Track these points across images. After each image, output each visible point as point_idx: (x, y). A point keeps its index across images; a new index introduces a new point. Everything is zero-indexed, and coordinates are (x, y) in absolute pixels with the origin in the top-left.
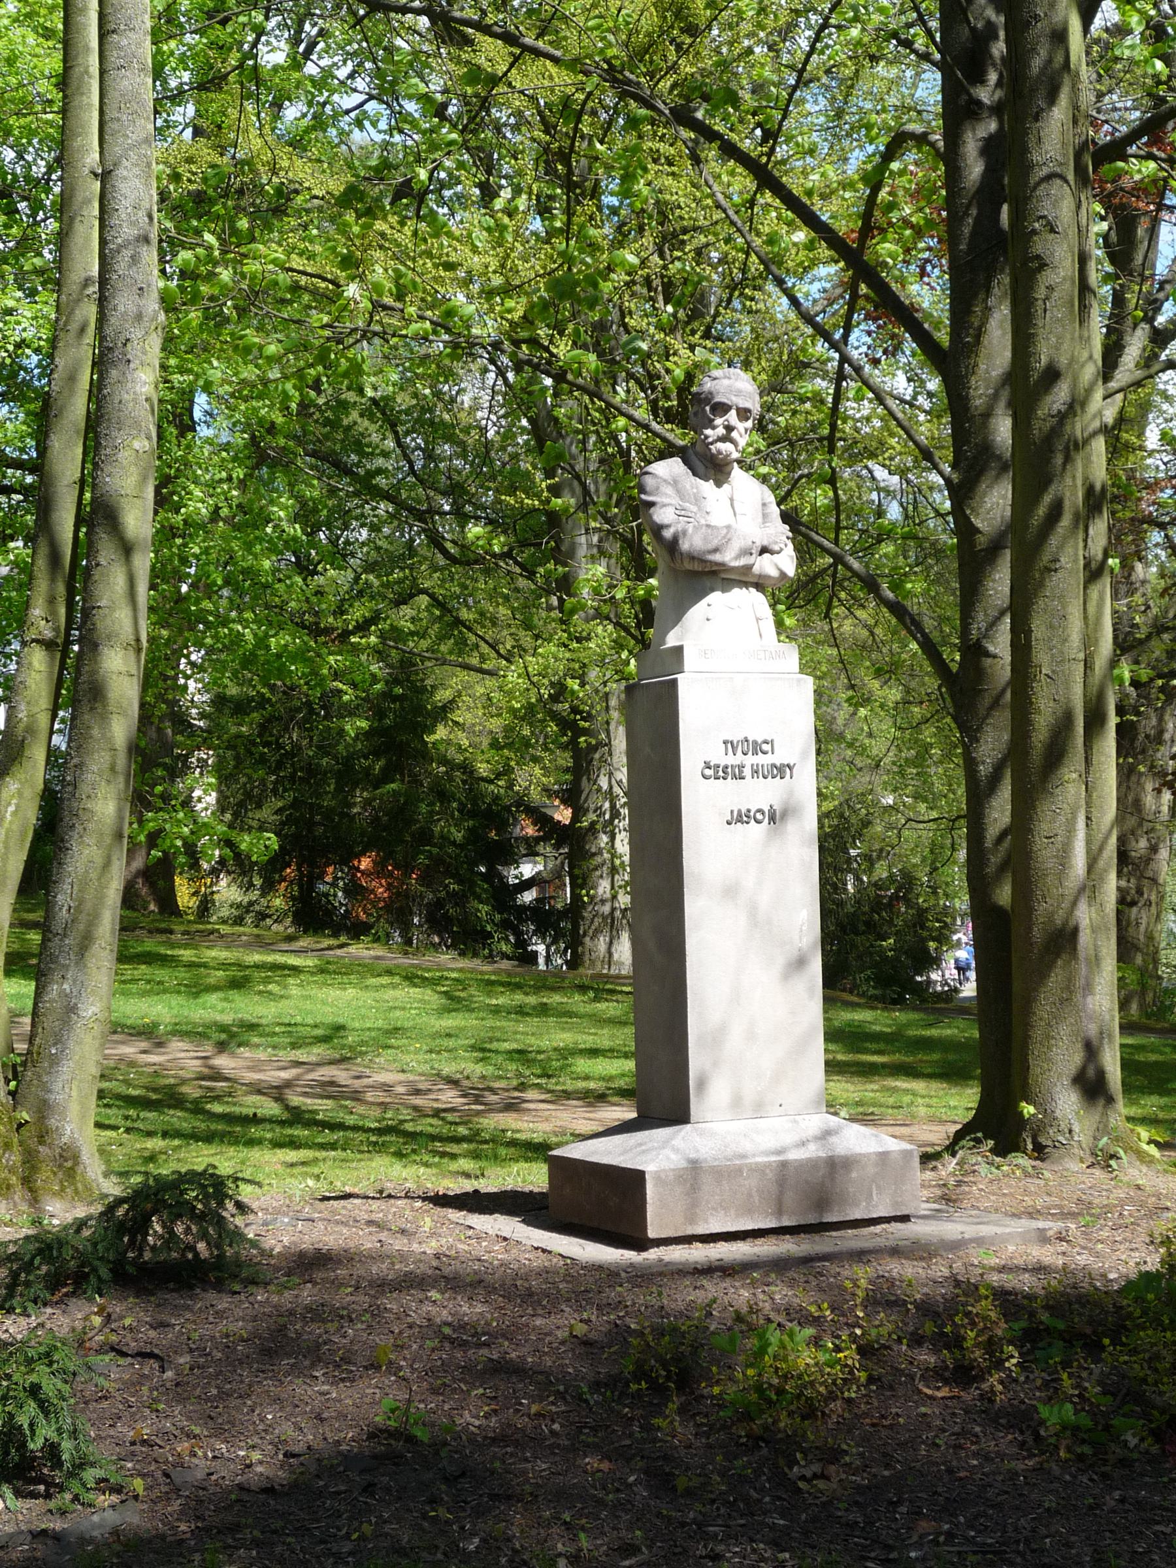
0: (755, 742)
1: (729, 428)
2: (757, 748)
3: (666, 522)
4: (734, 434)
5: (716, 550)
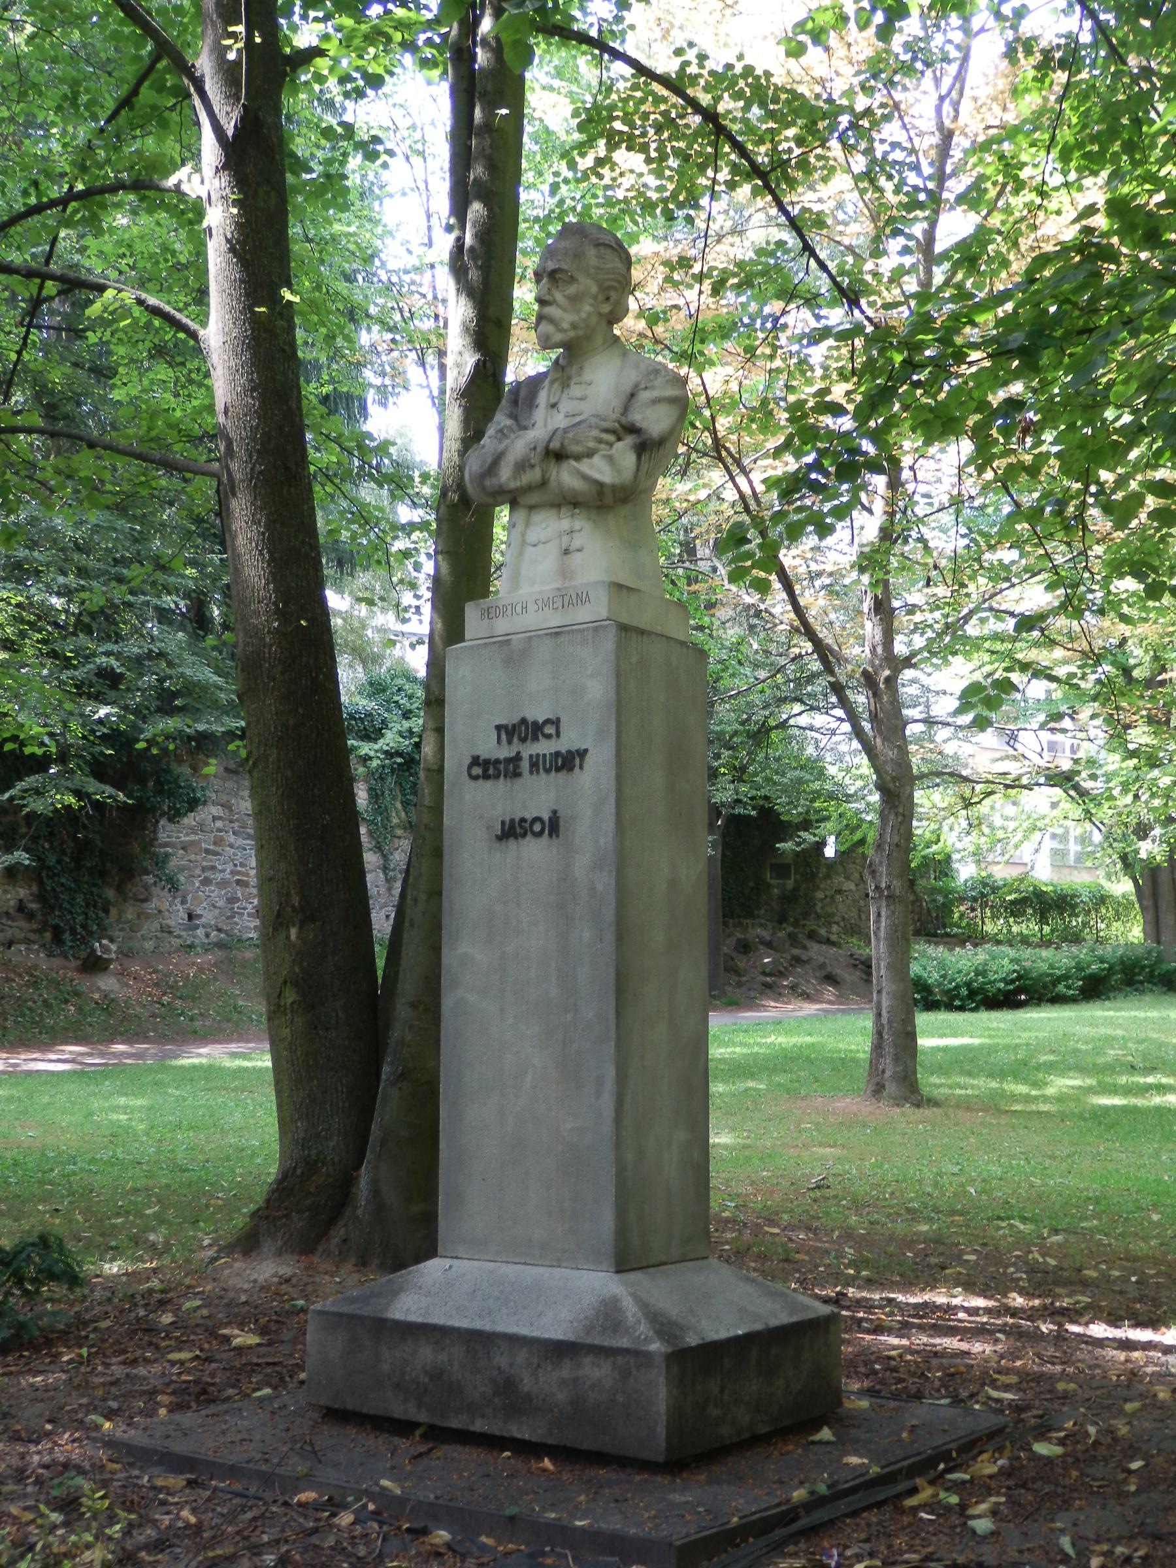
0: (535, 723)
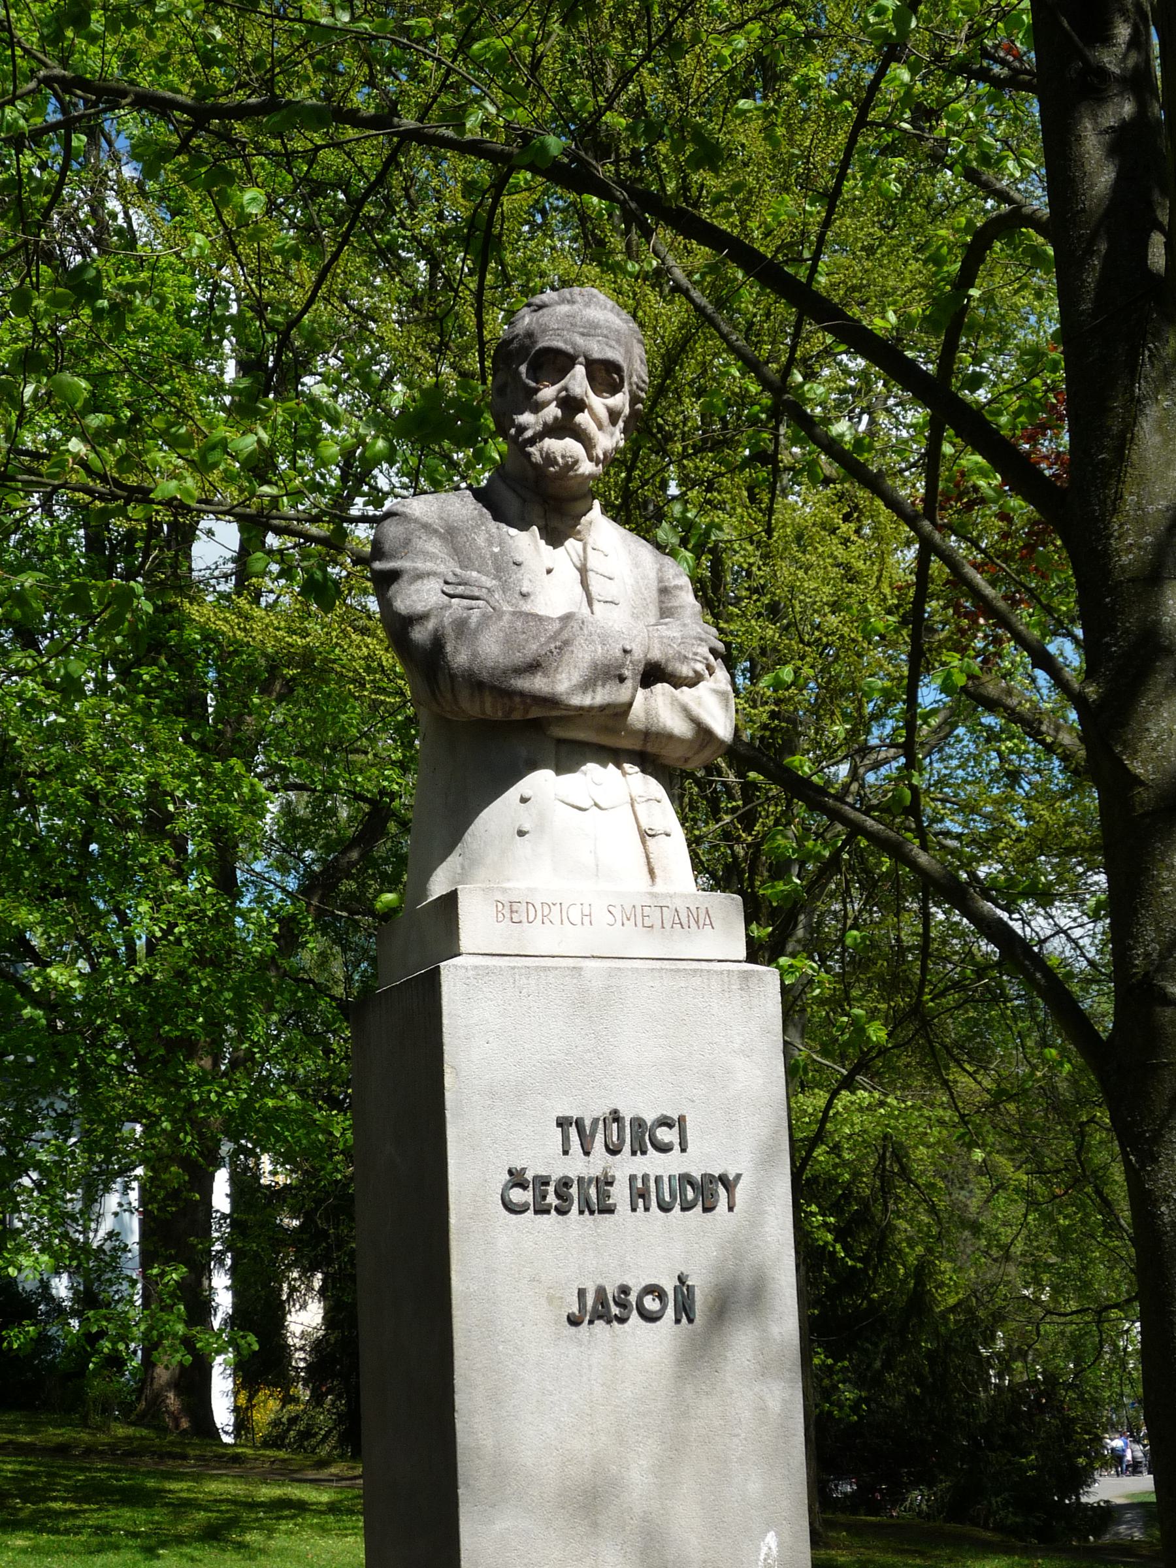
0: (638, 1123)
1: (572, 405)
2: (643, 1136)
3: (420, 608)
4: (583, 418)
5: (533, 667)
